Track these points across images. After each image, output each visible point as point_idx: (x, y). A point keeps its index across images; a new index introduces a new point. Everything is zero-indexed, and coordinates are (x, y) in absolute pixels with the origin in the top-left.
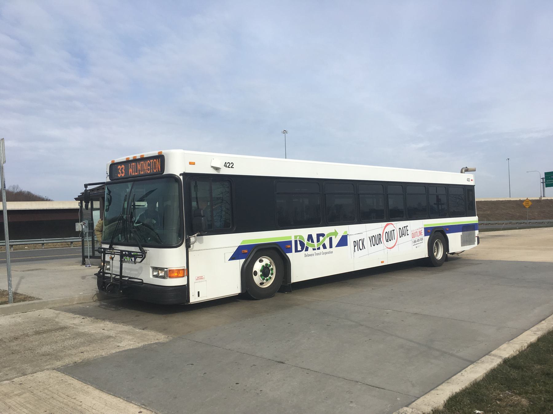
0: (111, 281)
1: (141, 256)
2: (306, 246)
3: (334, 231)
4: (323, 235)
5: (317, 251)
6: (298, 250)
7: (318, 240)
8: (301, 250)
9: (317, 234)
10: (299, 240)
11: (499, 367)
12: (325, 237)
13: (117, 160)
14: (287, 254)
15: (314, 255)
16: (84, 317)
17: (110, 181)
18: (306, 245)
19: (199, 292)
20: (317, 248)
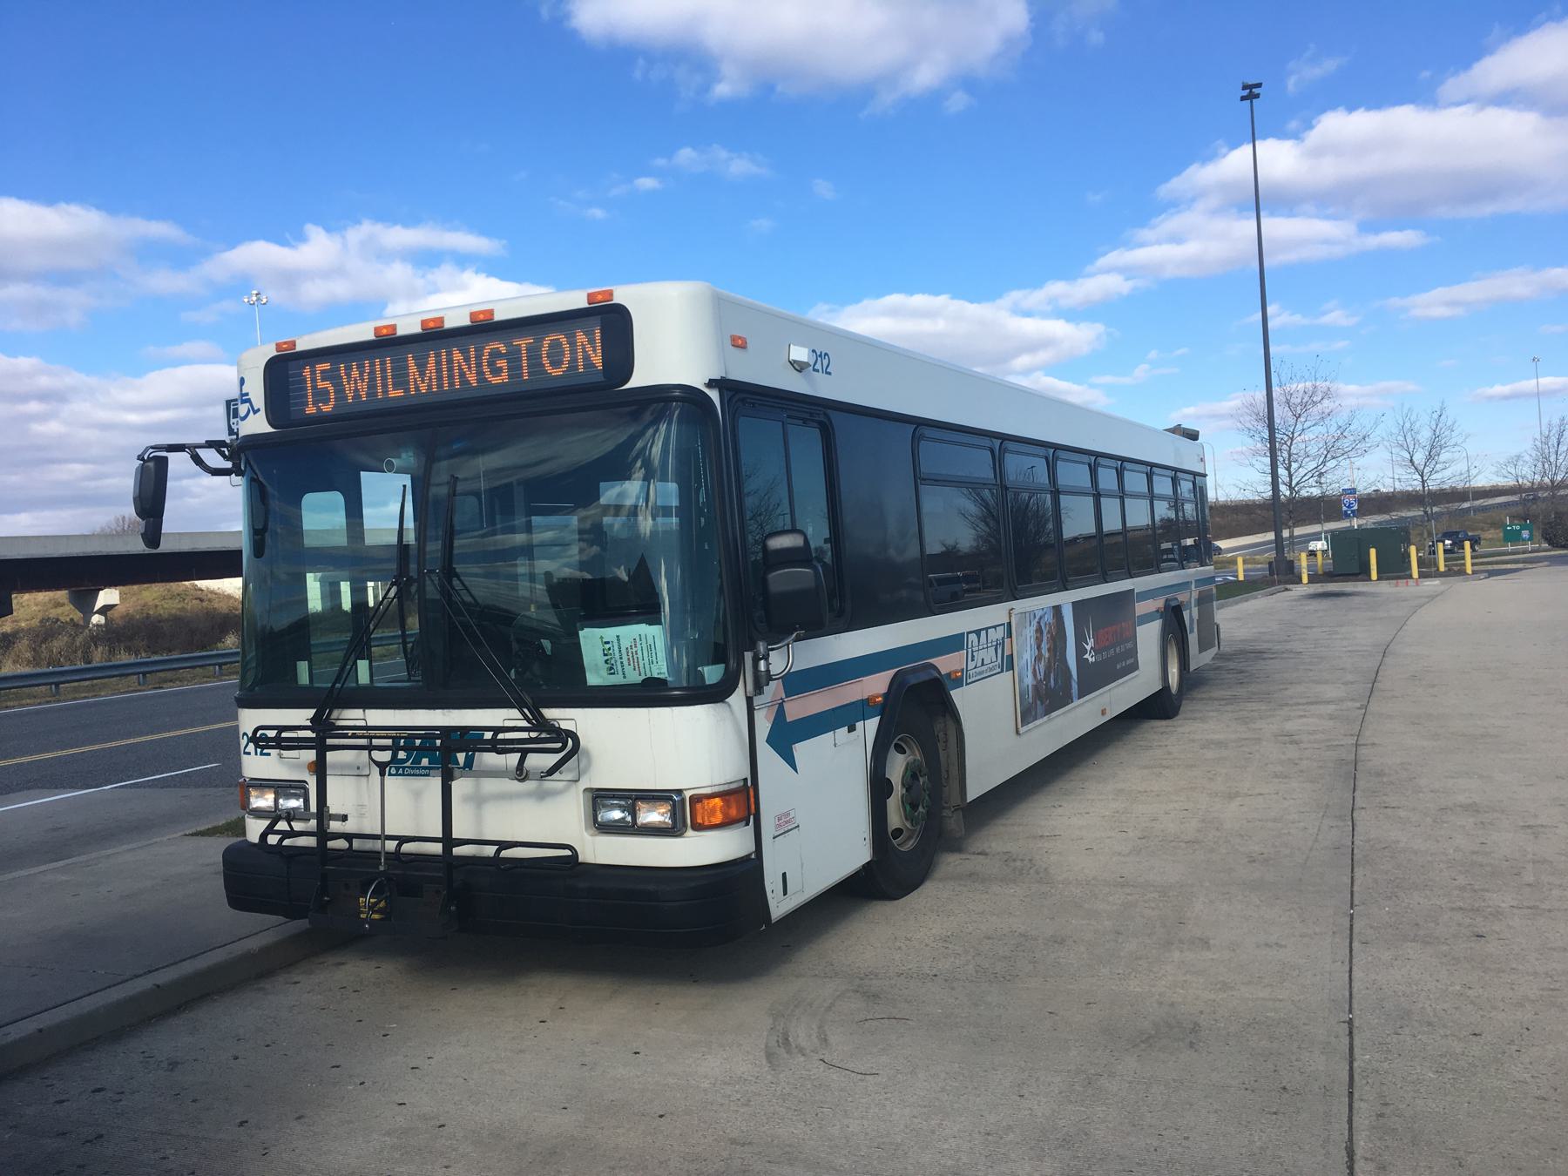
1: (559, 745)
13: (306, 342)
14: (314, 711)
17: (603, 379)
19: (784, 874)
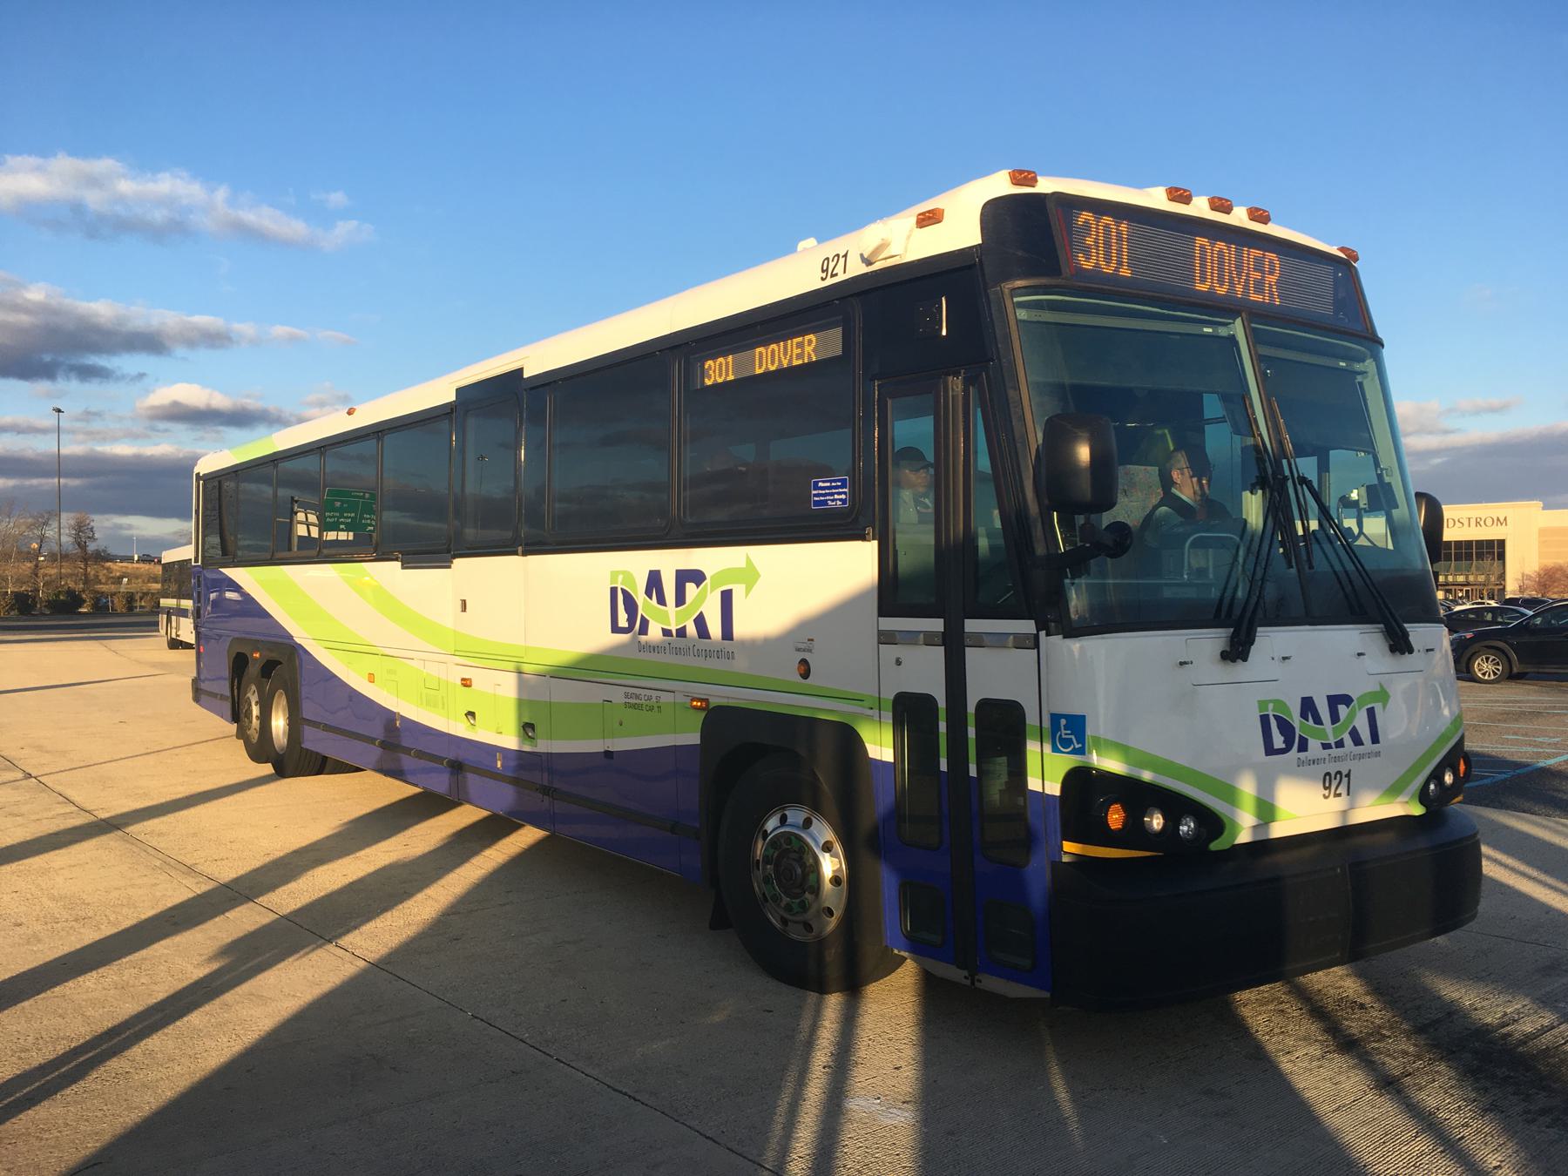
0: (698, 825)
2: (1300, 736)
3: (743, 565)
4: (697, 577)
5: (1335, 752)
6: (1275, 747)
7: (1335, 718)
8: (1284, 746)
9: (677, 571)
10: (1274, 715)
11: (771, 851)
12: (1354, 707)
15: (1327, 761)
16: (1510, 998)
18: (1298, 732)
20: (1336, 743)
